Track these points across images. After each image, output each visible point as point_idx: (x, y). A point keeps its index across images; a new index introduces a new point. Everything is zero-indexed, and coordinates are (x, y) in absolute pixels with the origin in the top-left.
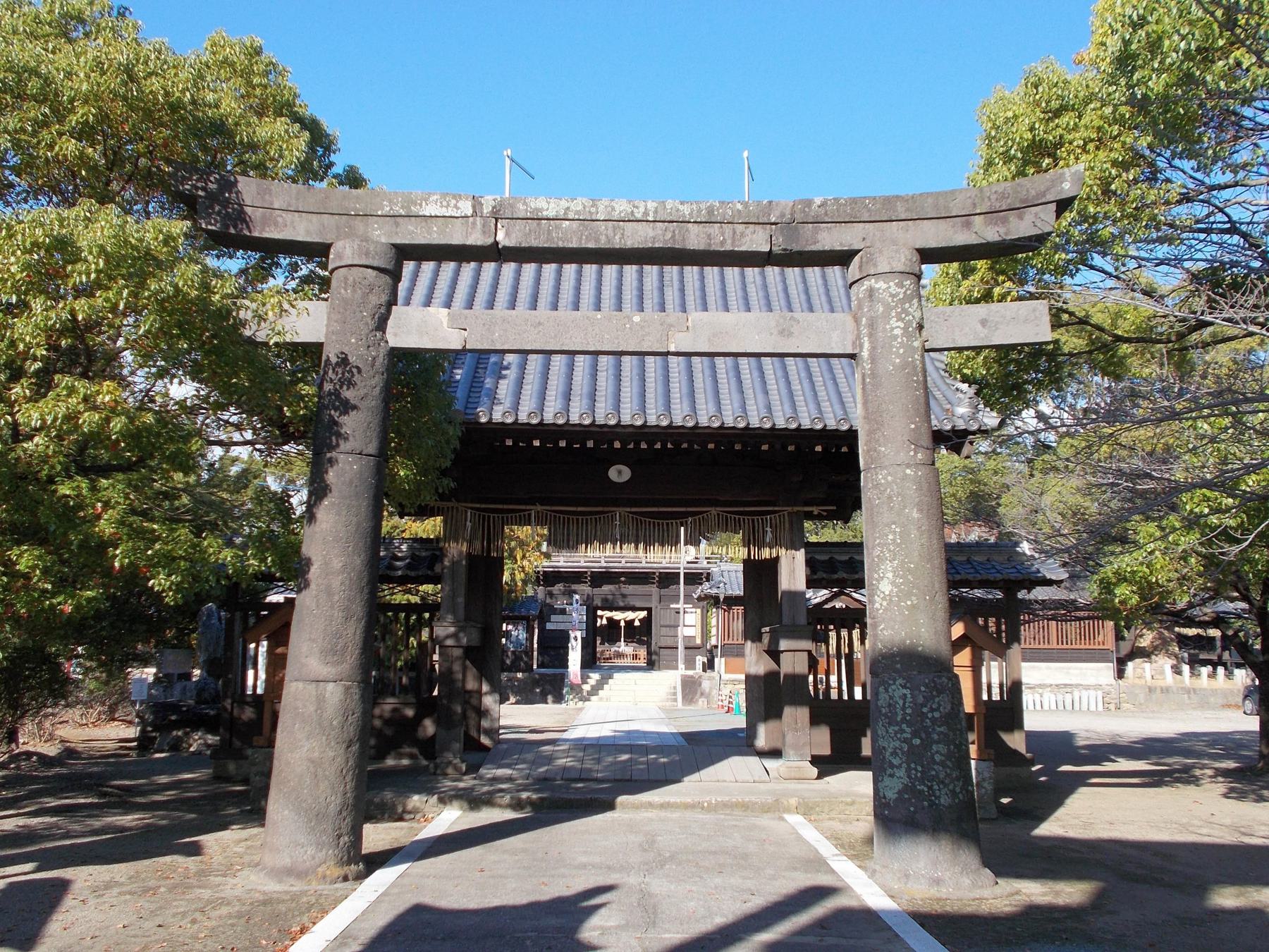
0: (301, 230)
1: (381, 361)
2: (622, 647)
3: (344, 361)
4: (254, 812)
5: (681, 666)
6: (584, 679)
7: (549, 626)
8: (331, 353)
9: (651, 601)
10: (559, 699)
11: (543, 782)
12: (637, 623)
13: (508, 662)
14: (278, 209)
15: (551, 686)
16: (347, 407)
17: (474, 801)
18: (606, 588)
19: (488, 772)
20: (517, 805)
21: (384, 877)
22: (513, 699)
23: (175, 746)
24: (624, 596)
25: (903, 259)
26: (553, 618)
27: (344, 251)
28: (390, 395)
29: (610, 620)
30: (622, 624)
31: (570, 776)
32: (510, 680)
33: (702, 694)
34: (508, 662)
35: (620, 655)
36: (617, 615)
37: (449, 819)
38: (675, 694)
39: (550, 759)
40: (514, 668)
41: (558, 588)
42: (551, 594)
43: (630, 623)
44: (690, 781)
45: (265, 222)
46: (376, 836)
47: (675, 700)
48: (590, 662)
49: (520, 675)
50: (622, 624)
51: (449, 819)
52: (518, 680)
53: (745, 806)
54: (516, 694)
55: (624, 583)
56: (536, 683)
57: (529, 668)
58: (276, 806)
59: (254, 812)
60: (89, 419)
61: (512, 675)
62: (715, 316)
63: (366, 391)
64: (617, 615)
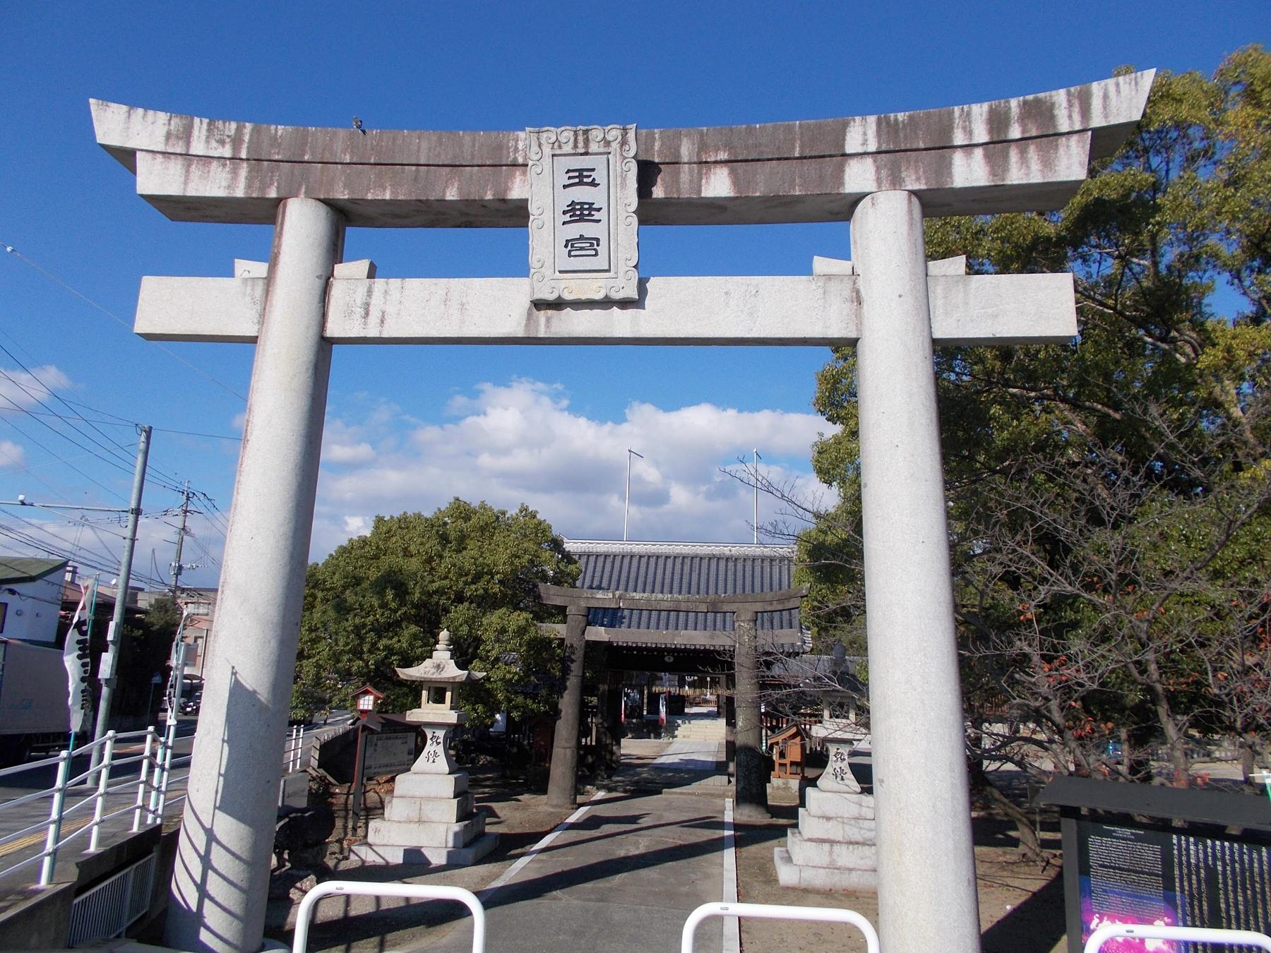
0: (558, 602)
1: (583, 644)
3: (572, 646)
4: (543, 791)
8: (567, 642)
10: (658, 736)
11: (637, 783)
14: (552, 595)
15: (652, 729)
16: (573, 661)
17: (610, 790)
19: (615, 779)
20: (625, 791)
21: (583, 810)
23: (472, 761)
25: (749, 616)
27: (571, 610)
28: (586, 654)
31: (647, 781)
37: (601, 795)
39: (639, 774)
44: (695, 785)
45: (548, 598)
46: (580, 799)
51: (601, 795)
53: (712, 795)
54: (632, 732)
57: (641, 716)
58: (551, 787)
59: (543, 791)
60: (508, 676)
62: (691, 632)
63: (578, 656)
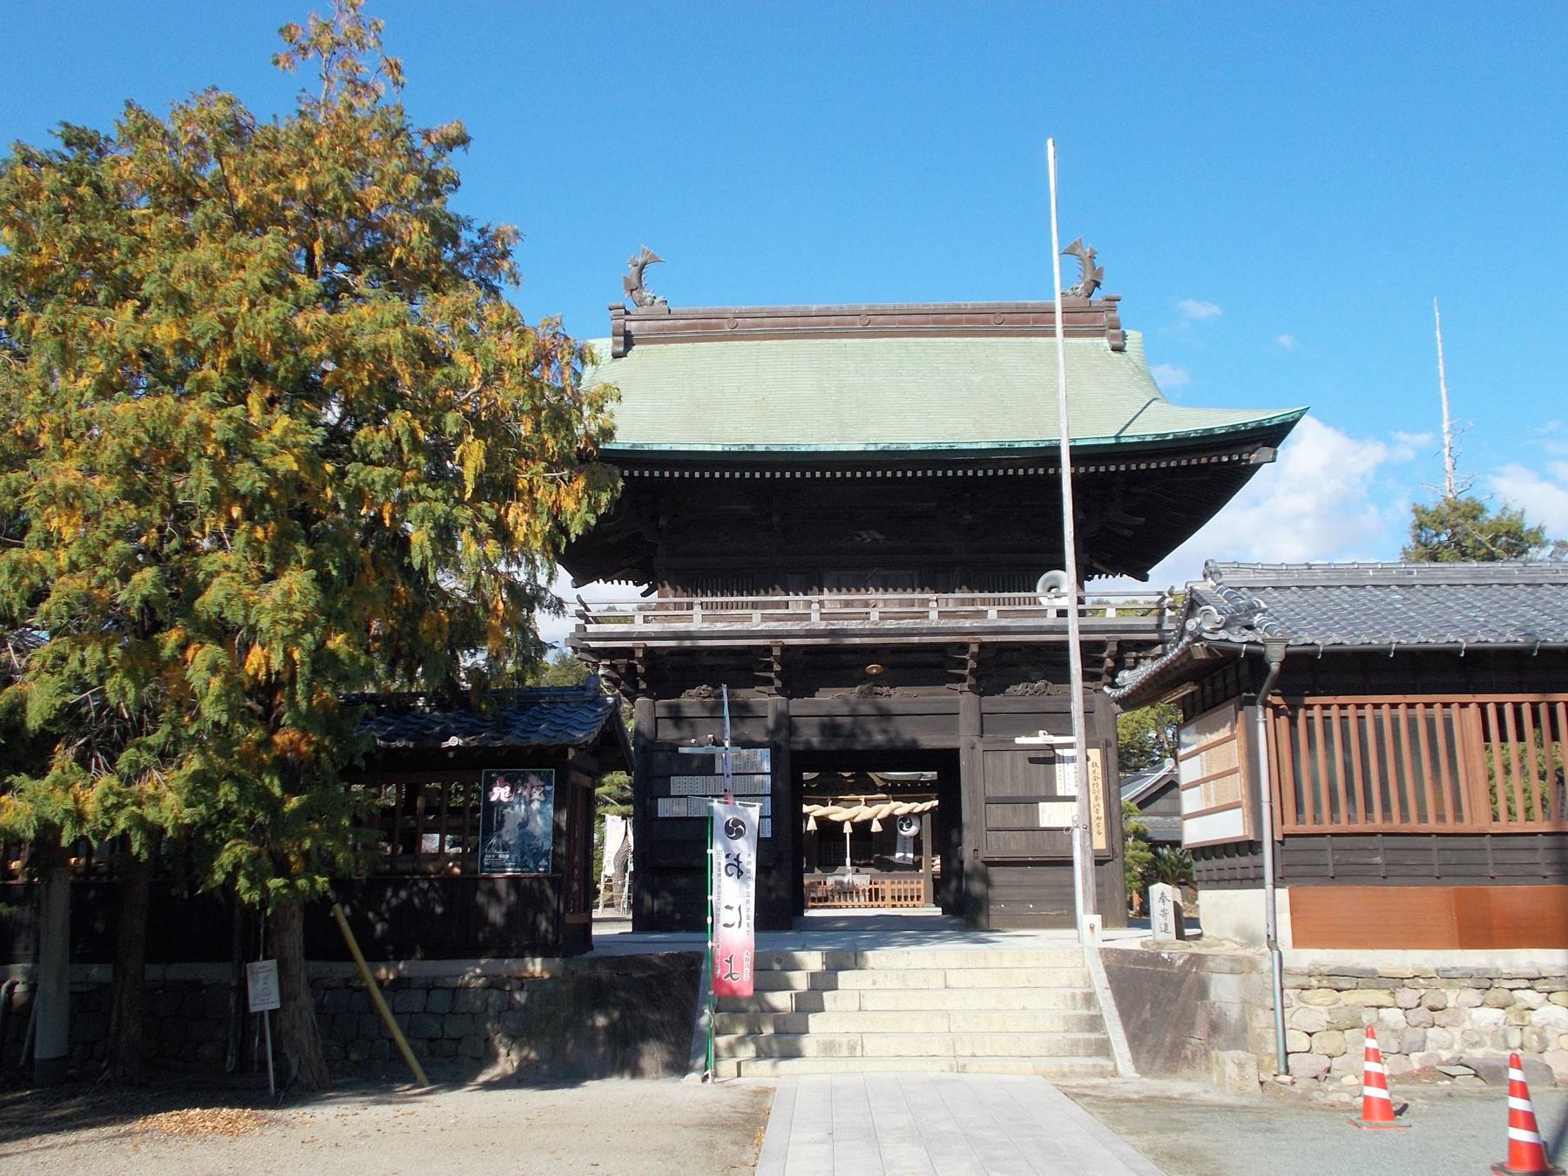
2: (849, 875)
5: (1087, 917)
6: (769, 972)
7: (667, 808)
9: (954, 730)
12: (876, 827)
13: (496, 914)
18: (829, 699)
22: (507, 1061)
24: (885, 715)
26: (678, 784)
29: (821, 821)
30: (848, 829)
32: (495, 983)
33: (1215, 1028)
34: (496, 914)
35: (847, 892)
36: (837, 813)
38: (1095, 1023)
40: (514, 940)
41: (691, 701)
42: (677, 717)
43: (862, 828)
47: (1103, 1048)
48: (780, 911)
49: (536, 966)
50: (848, 829)
52: (523, 982)
55: (877, 680)
56: (595, 995)
61: (509, 965)
64: (837, 813)
